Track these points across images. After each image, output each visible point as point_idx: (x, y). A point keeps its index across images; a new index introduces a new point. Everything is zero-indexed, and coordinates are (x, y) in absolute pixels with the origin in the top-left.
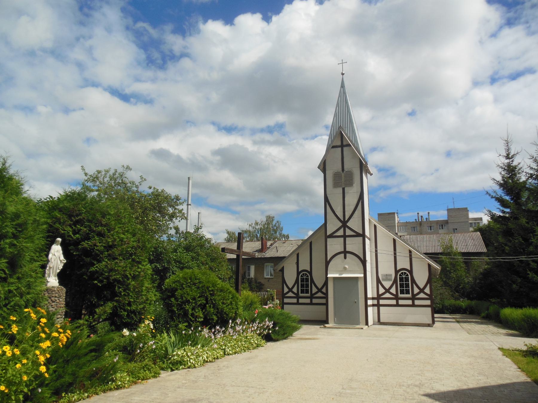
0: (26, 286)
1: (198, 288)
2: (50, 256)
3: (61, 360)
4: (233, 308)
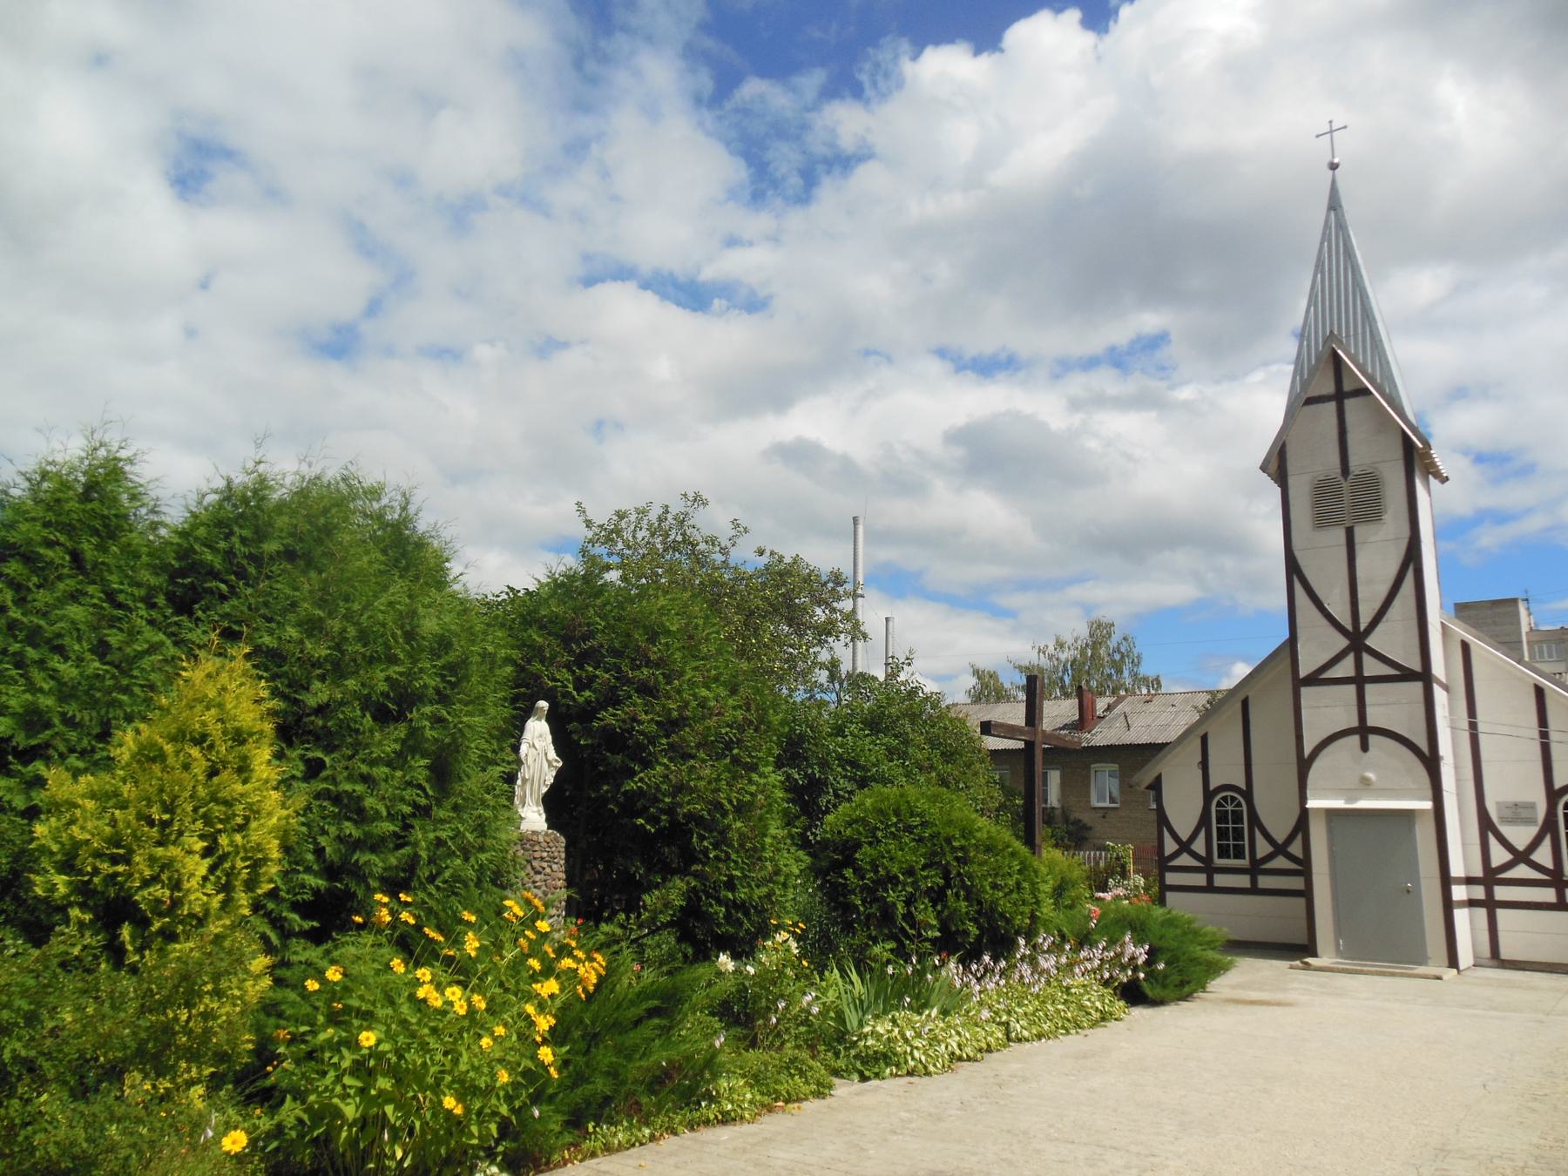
0: (475, 830)
1: (920, 840)
2: (524, 748)
3: (577, 1034)
4: (1024, 902)
